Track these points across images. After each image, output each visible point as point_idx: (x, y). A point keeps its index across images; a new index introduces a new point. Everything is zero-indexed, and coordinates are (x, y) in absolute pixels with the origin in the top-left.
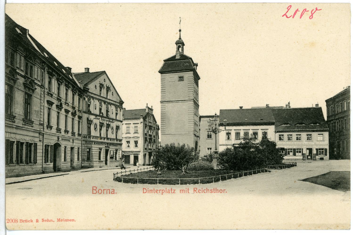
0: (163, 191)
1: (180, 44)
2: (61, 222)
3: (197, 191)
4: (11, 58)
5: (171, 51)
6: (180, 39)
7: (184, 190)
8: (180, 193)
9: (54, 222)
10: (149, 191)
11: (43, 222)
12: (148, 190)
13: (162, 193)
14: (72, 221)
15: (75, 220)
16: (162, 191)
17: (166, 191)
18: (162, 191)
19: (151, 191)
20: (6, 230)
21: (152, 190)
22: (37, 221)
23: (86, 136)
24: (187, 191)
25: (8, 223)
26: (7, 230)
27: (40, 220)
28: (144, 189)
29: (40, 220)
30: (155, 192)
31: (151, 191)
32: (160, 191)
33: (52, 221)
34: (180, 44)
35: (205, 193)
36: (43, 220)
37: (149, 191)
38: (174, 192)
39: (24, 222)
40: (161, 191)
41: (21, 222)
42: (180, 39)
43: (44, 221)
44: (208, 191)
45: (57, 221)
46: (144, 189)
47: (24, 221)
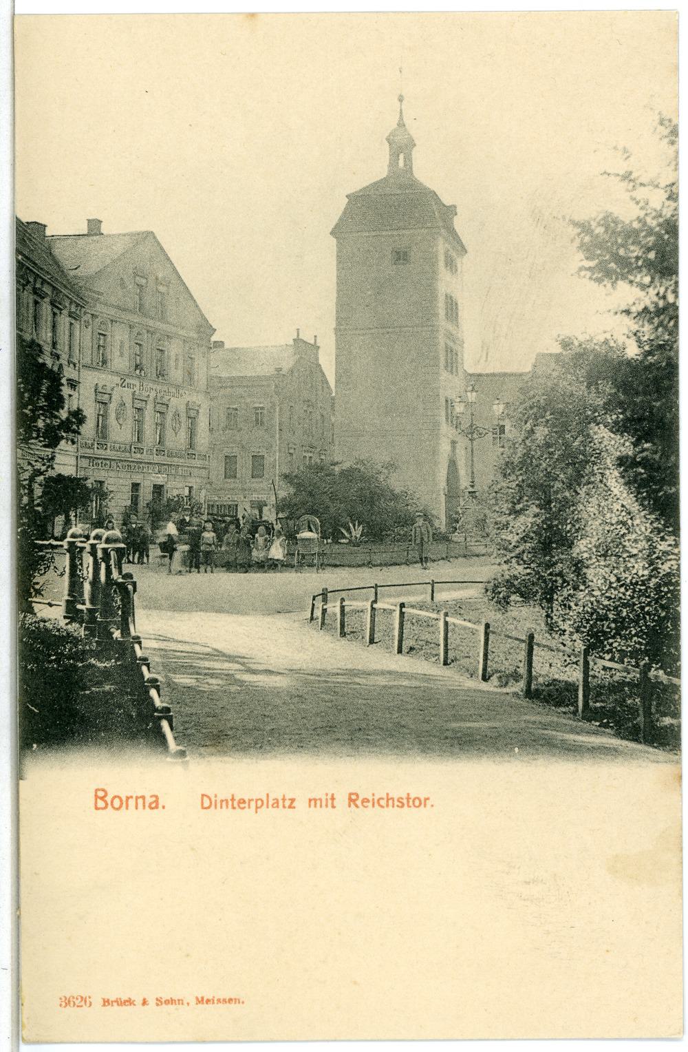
0: (259, 803)
1: (401, 146)
2: (205, 1005)
3: (359, 802)
4: (212, 678)
5: (376, 169)
6: (401, 124)
7: (321, 800)
8: (310, 806)
9: (245, 1005)
10: (219, 805)
11: (159, 1007)
12: (216, 801)
13: (257, 808)
14: (172, 1004)
15: (241, 1001)
16: (256, 802)
17: (268, 802)
18: (256, 802)
19: (224, 803)
20: (18, 1043)
21: (227, 800)
22: (145, 1002)
23: (90, 442)
24: (330, 802)
25: (81, 1008)
26: (21, 1042)
27: (152, 1002)
28: (205, 798)
29: (152, 1002)
30: (236, 805)
31: (224, 803)
32: (249, 803)
33: (239, 1003)
34: (401, 146)
35: (382, 807)
36: (159, 1002)
37: (219, 805)
38: (293, 805)
39: (112, 1006)
40: (253, 804)
41: (107, 1004)
42: (401, 124)
43: (161, 1002)
44: (390, 802)
45: (197, 1004)
46: (205, 798)
47: (112, 1002)
